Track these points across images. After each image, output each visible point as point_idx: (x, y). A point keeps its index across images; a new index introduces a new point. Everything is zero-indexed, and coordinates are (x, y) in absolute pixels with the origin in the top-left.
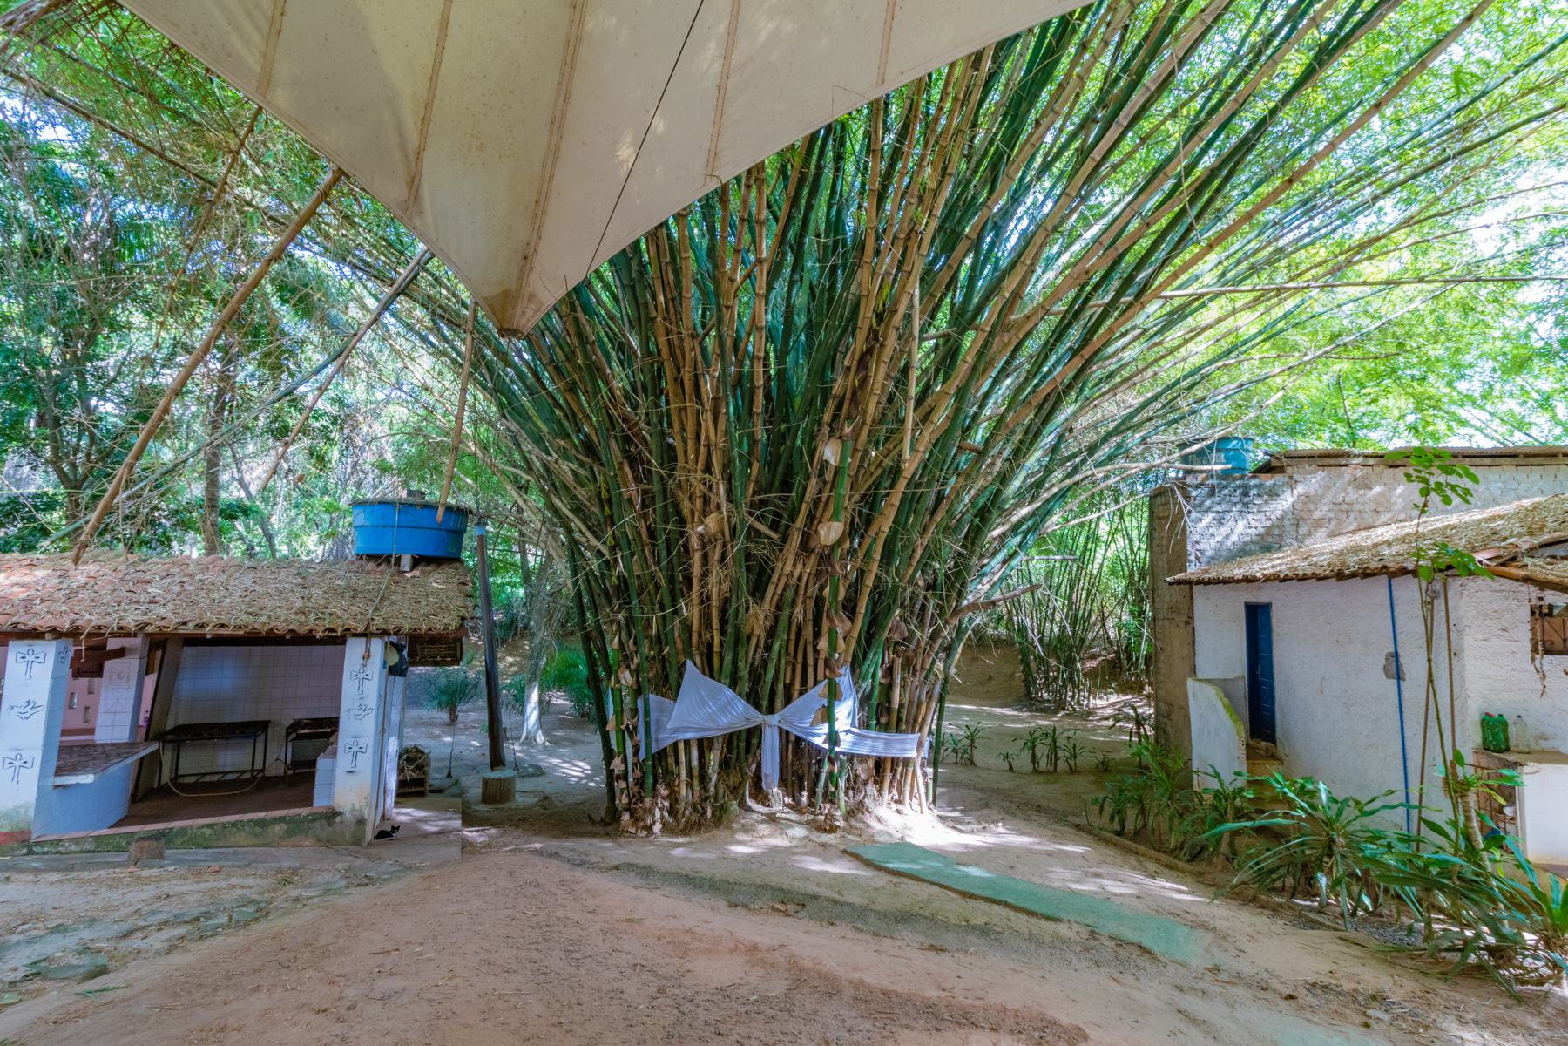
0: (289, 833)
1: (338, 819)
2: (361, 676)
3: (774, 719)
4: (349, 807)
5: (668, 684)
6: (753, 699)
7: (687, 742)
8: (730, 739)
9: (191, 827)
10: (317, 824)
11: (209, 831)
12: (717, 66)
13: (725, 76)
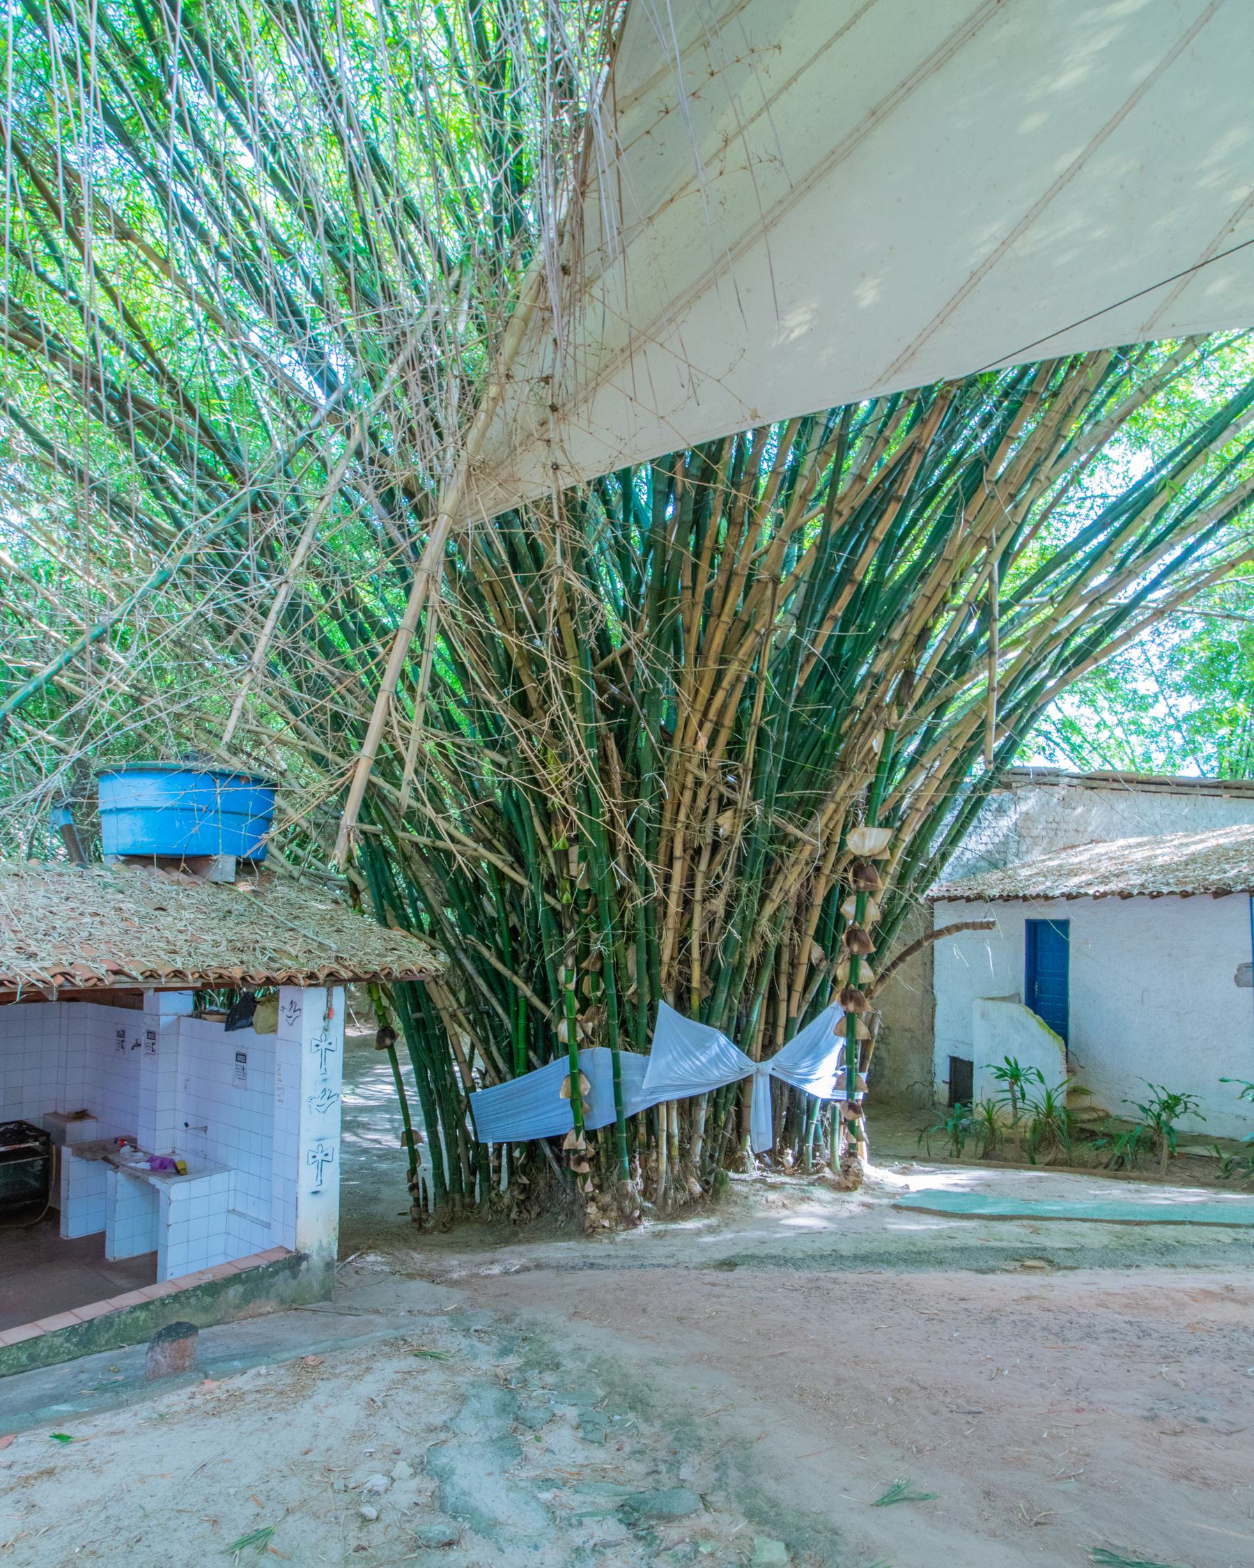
0: (248, 1298)
1: (304, 1265)
2: (324, 1045)
3: (768, 1066)
4: (316, 1245)
5: (633, 1031)
6: (739, 1035)
7: (668, 1104)
8: (717, 1098)
9: (119, 1312)
10: (280, 1278)
11: (142, 1315)
12: (987, 249)
13: (989, 263)
